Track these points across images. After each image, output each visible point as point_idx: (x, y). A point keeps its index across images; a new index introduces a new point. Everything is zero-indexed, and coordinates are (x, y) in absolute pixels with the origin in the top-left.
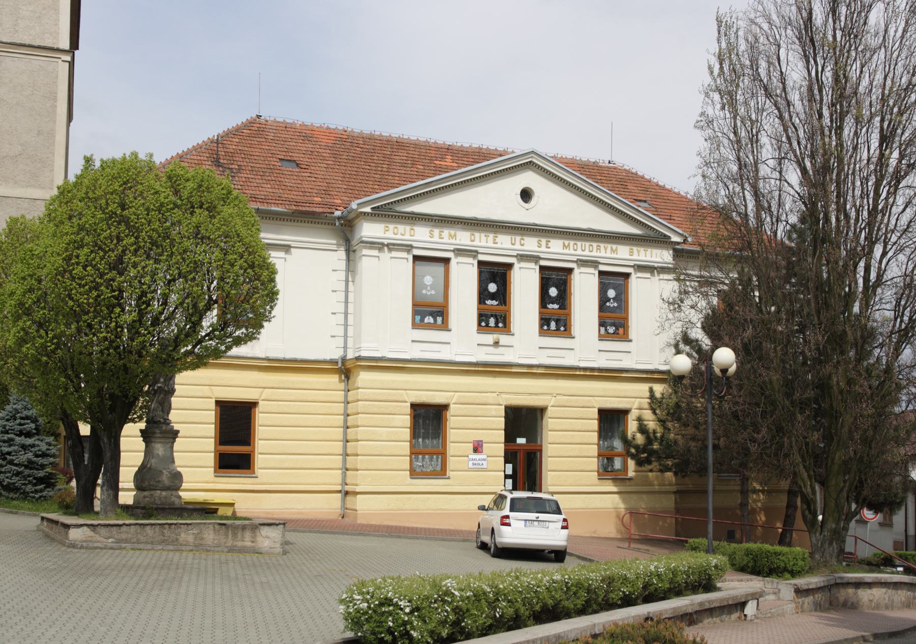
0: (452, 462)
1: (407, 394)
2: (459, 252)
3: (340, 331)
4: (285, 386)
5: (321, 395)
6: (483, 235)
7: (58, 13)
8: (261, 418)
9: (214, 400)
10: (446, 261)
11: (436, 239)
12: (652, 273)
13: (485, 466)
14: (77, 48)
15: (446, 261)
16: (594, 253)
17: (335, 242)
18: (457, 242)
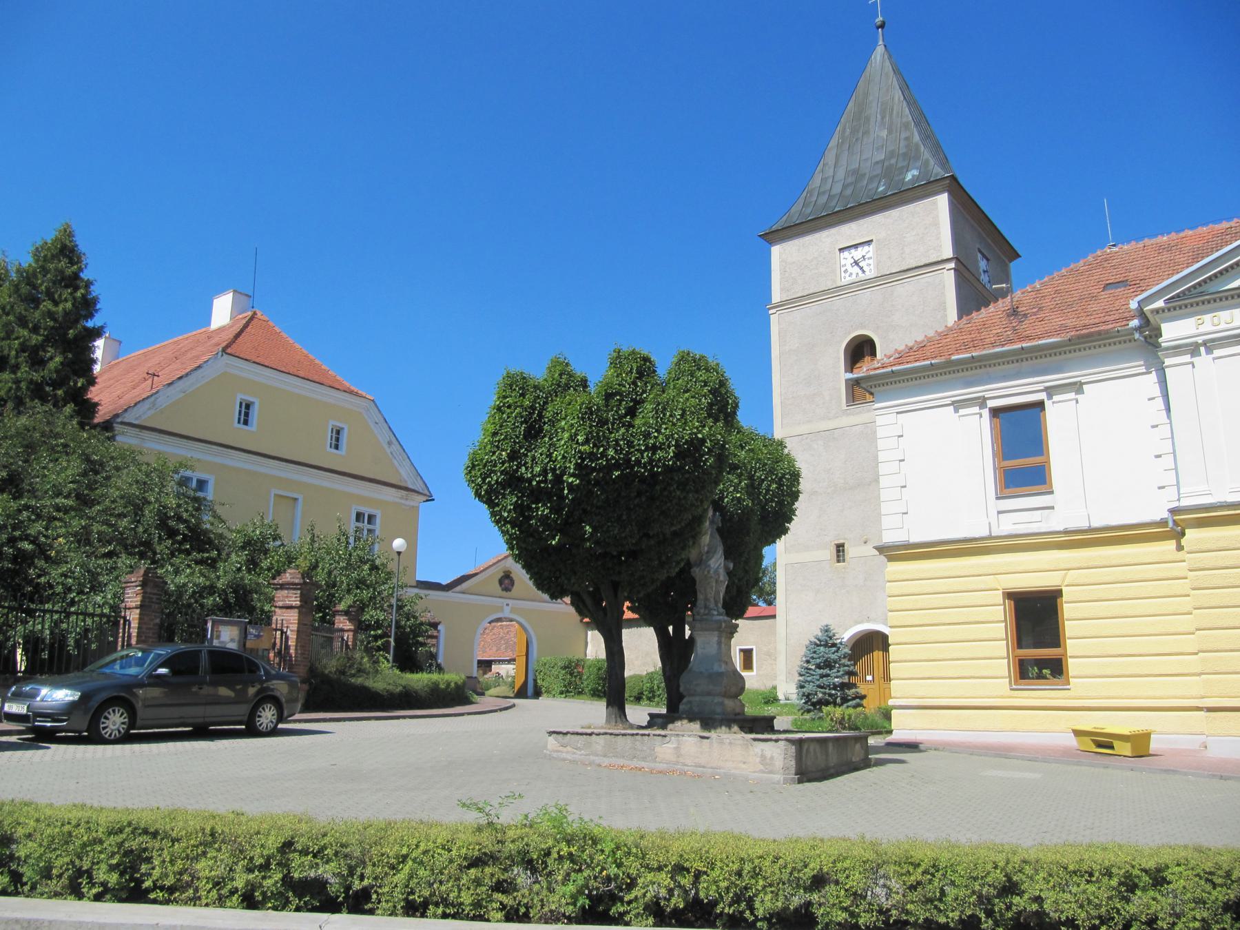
3: (1170, 478)
4: (1096, 564)
5: (1152, 571)
7: (939, 227)
8: (1068, 610)
9: (1000, 592)
17: (1142, 363)
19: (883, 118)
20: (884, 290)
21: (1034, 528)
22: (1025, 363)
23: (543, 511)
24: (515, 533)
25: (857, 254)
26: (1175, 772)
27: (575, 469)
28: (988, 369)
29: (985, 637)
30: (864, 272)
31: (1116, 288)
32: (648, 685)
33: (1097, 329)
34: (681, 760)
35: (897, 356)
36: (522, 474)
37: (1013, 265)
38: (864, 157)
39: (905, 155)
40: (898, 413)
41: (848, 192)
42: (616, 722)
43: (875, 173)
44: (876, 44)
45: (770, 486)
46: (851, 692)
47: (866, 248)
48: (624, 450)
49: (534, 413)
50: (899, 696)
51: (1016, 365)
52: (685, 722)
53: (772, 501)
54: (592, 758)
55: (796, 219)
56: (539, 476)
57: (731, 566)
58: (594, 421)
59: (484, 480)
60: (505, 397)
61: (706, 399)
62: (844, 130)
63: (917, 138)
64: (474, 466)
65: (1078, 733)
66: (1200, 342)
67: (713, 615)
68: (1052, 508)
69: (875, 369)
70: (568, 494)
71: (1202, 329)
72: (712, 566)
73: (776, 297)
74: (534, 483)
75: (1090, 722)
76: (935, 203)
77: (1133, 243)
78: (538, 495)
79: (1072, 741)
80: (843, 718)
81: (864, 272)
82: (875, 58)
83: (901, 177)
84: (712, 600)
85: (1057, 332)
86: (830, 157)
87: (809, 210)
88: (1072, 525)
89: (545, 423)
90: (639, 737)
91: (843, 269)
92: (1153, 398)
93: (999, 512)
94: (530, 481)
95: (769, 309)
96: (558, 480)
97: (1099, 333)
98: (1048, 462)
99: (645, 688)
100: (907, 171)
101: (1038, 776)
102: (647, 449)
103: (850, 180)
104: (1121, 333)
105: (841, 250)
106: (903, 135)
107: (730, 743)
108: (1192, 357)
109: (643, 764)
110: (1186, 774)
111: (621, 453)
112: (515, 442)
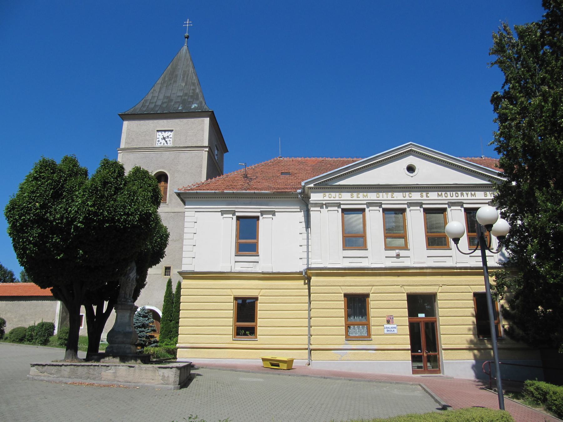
0: (373, 329)
1: (341, 288)
2: (369, 204)
6: (384, 194)
8: (259, 306)
9: (233, 297)
10: (363, 210)
11: (355, 198)
12: (322, 207)
13: (396, 332)
14: (227, 151)
15: (363, 210)
16: (460, 197)
18: (369, 198)
19: (183, 77)
20: (175, 153)
21: (249, 270)
22: (254, 199)
23: (56, 240)
24: (35, 250)
25: (166, 134)
26: (306, 376)
27: (83, 219)
28: (238, 199)
29: (224, 316)
30: (167, 143)
31: (286, 175)
32: (29, 333)
33: (284, 190)
34: (117, 379)
35: (197, 186)
36: (47, 217)
37: (225, 155)
38: (173, 92)
39: (192, 96)
40: (196, 212)
41: (164, 105)
42: (72, 358)
43: (178, 101)
44: (183, 45)
45: (157, 239)
46: (152, 340)
47: (170, 133)
48: (112, 213)
49: (59, 184)
50: (181, 342)
51: (250, 199)
52: (111, 358)
53: (157, 247)
54: (61, 379)
55: (138, 111)
56: (58, 220)
57: (138, 277)
58: (99, 195)
59: (20, 217)
60: (41, 172)
61: (150, 193)
62: (165, 77)
63: (198, 91)
64: (13, 208)
65: (264, 360)
66: (324, 203)
67: (128, 302)
68: (258, 262)
69: (188, 190)
70: (73, 232)
71: (325, 198)
72: (131, 276)
73: (122, 146)
74: (55, 223)
75: (269, 355)
76: (203, 121)
77: (288, 158)
78: (55, 230)
79: (261, 363)
80: (154, 353)
81: (167, 143)
82: (183, 50)
83: (190, 106)
84: (128, 294)
85: (269, 188)
86: (157, 87)
87: (144, 109)
88: (266, 270)
89: (64, 191)
90: (92, 367)
91: (157, 140)
92: (301, 222)
93: (235, 262)
94: (51, 222)
95: (119, 150)
96: (70, 222)
97: (286, 192)
98: (258, 243)
99: (27, 334)
100: (192, 104)
101: (261, 380)
102: (125, 214)
103: (165, 100)
104: (293, 194)
105: (158, 131)
106: (192, 88)
107: (146, 370)
108: (320, 209)
109: (93, 382)
110: (311, 377)
111: (110, 214)
112: (46, 199)
